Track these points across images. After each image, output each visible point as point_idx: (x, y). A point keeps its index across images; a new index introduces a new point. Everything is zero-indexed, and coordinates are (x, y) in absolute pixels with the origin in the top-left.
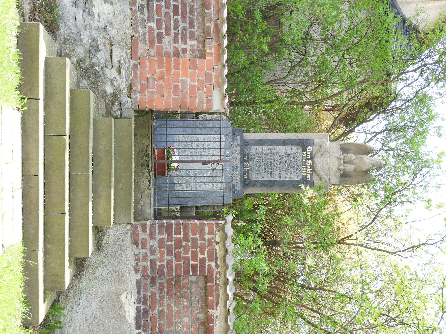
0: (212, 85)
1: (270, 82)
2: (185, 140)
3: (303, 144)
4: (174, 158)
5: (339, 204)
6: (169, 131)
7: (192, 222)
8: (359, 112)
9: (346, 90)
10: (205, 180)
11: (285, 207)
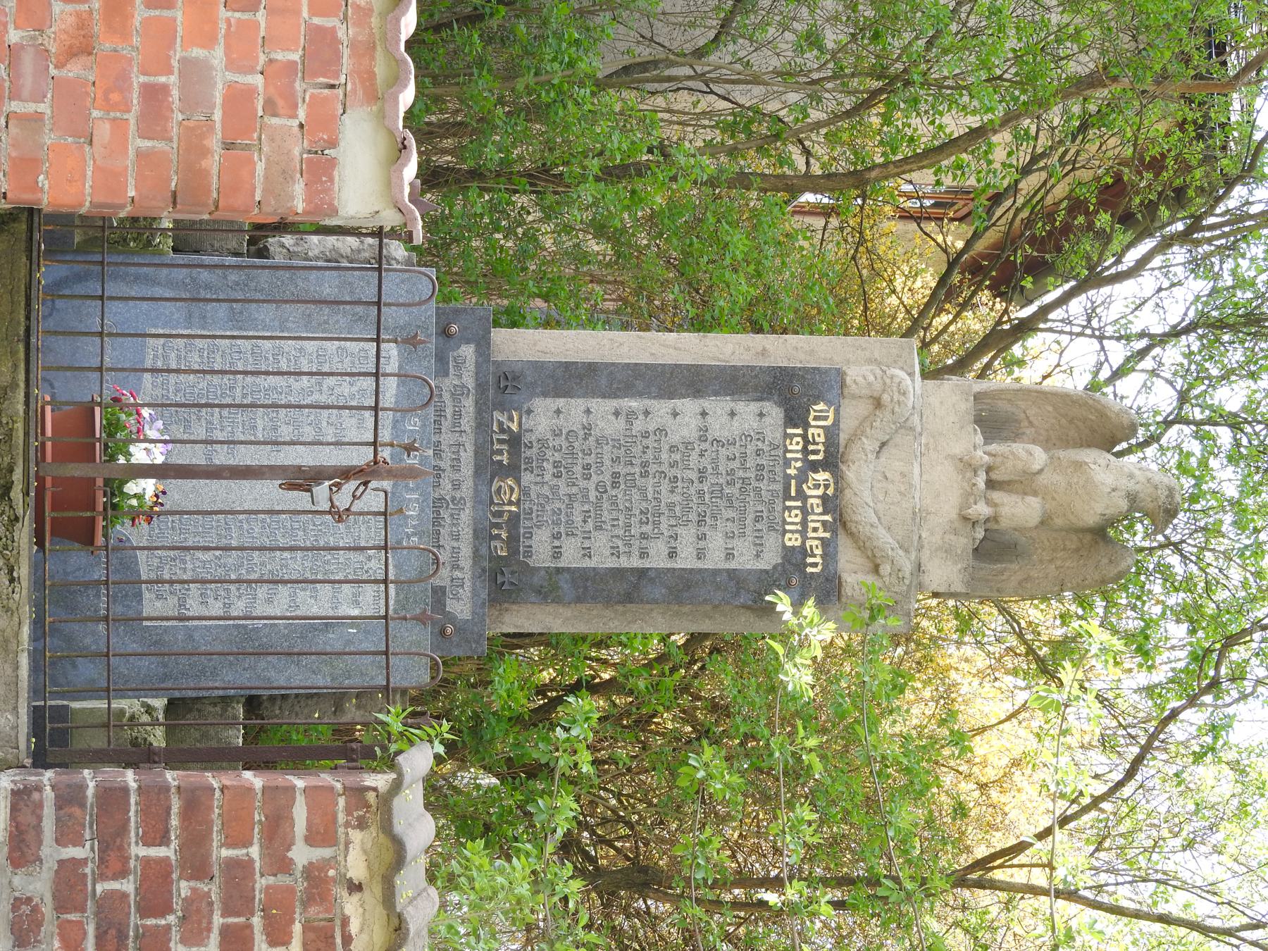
0: (340, 92)
1: (629, 75)
2: (195, 362)
3: (792, 392)
4: (139, 454)
5: (964, 689)
6: (117, 315)
7: (228, 779)
8: (1066, 229)
9: (1005, 122)
10: (297, 565)
11: (699, 698)
